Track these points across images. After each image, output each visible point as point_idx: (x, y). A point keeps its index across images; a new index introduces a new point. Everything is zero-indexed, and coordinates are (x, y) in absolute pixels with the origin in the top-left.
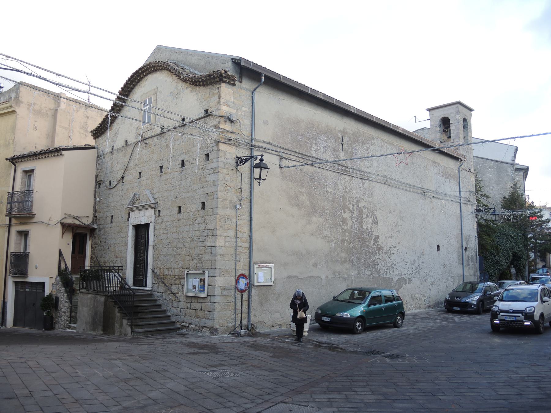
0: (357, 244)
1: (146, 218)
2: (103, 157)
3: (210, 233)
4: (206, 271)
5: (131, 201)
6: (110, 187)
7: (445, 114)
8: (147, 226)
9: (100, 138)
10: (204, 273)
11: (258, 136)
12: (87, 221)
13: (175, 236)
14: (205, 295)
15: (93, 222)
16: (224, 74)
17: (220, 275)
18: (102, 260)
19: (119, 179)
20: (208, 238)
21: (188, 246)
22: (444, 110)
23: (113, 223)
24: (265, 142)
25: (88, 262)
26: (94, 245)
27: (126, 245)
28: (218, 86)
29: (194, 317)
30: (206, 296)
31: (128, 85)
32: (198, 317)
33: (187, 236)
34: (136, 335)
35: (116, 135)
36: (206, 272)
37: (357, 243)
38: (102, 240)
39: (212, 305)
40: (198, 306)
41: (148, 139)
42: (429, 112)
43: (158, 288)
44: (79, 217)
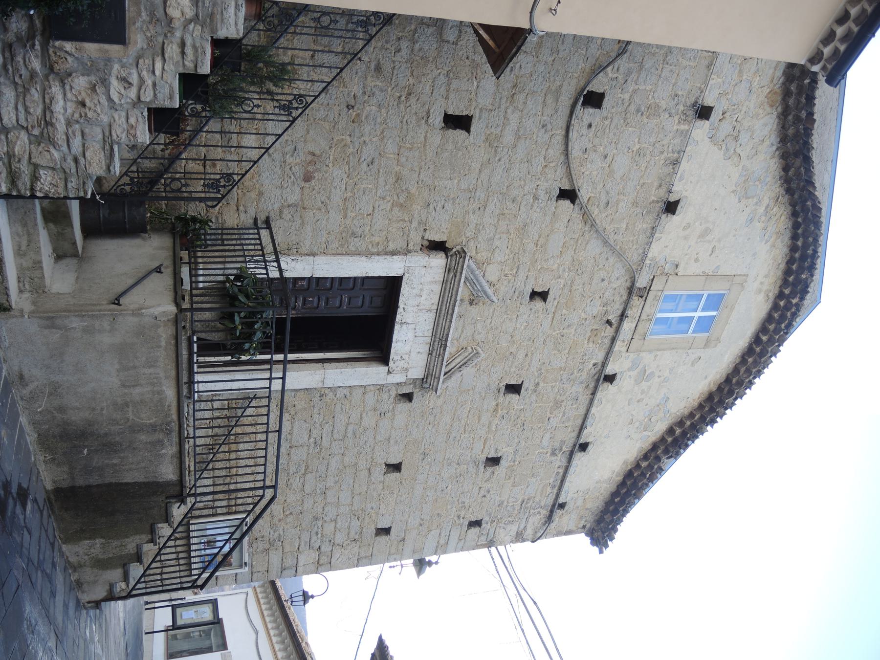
1: (407, 348)
21: (305, 508)
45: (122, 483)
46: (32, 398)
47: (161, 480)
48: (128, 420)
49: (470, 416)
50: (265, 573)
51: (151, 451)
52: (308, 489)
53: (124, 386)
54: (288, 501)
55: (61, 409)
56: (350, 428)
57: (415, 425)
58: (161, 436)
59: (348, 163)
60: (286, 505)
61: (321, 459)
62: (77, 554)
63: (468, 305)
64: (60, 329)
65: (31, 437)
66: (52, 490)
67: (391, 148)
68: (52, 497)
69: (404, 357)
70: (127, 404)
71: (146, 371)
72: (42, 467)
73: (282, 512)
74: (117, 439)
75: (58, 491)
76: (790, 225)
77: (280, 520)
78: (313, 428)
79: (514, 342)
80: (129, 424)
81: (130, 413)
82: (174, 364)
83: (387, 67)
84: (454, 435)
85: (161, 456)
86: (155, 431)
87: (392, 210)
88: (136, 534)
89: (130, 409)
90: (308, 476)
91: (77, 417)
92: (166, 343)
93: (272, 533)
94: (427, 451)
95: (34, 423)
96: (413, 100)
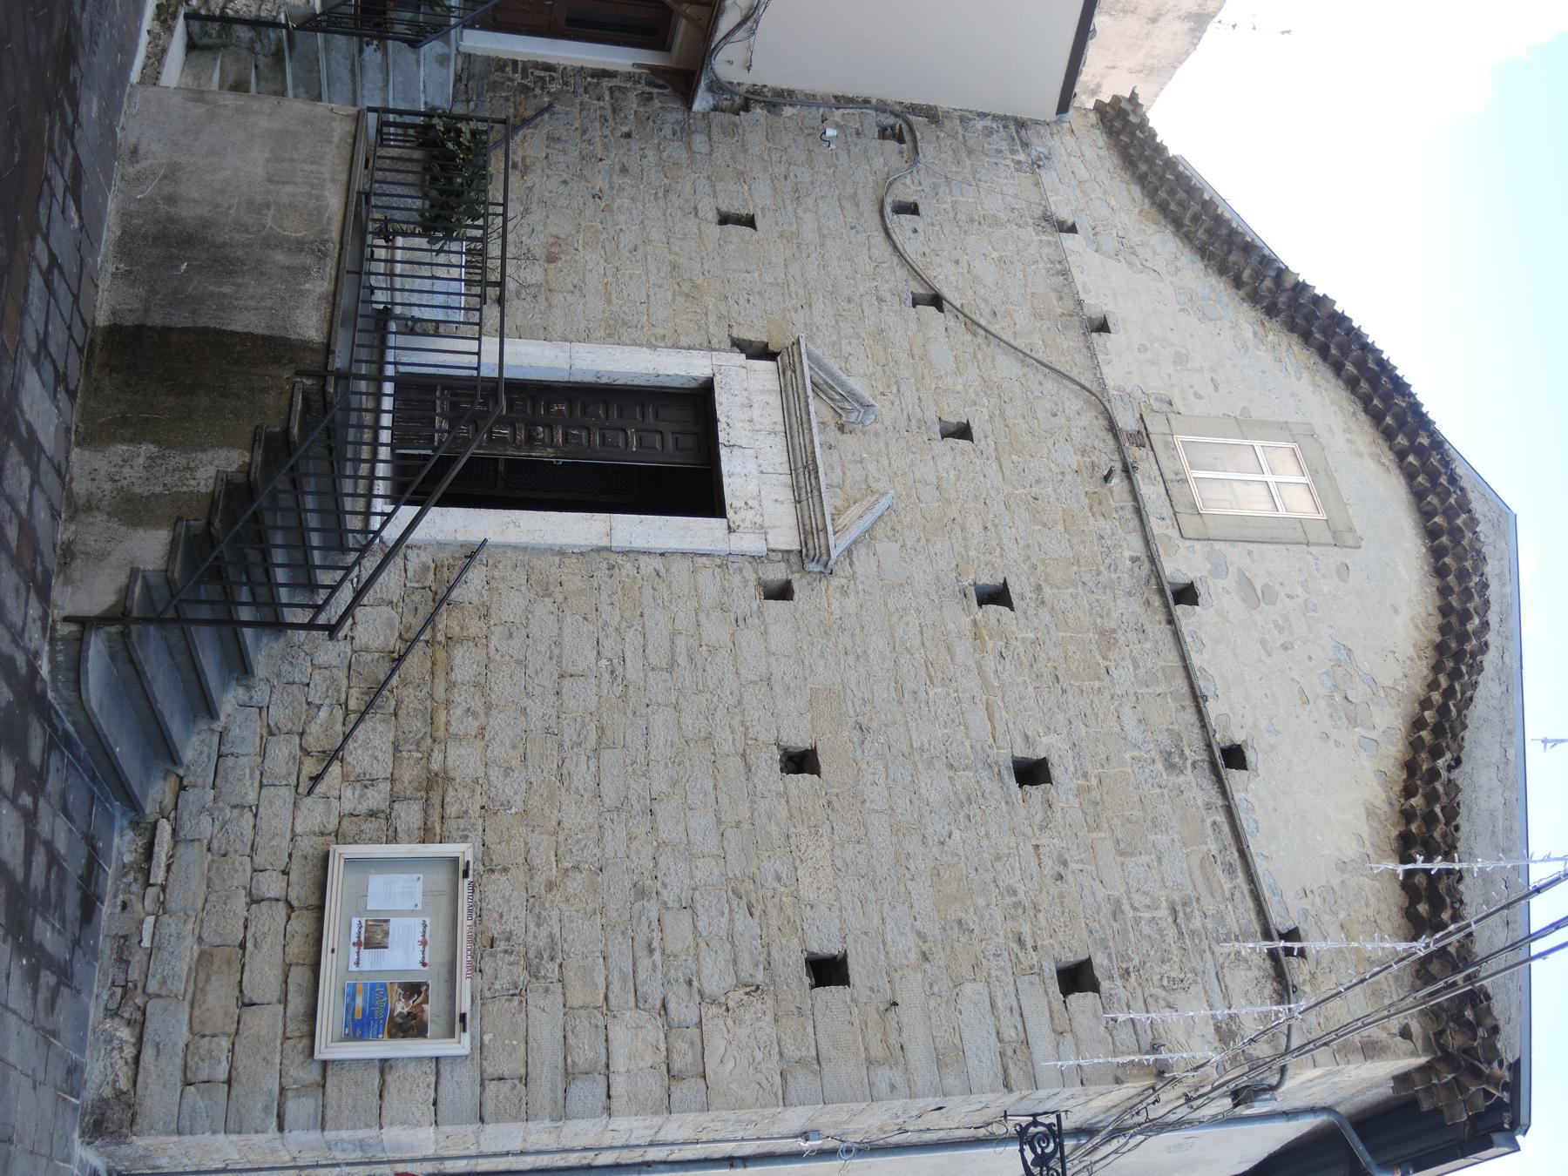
1: (752, 488)
2: (1022, 157)
4: (466, 1037)
5: (831, 375)
6: (888, 209)
9: (1101, 139)
10: (457, 1023)
12: (730, 62)
13: (661, 722)
14: (328, 1048)
15: (717, 87)
18: (529, 145)
19: (929, 274)
20: (653, 1032)
21: (610, 853)
23: (715, 231)
25: (527, 50)
26: (611, 90)
27: (614, 332)
29: (200, 939)
30: (328, 1048)
31: (1356, 352)
32: (202, 976)
33: (664, 836)
34: (60, 658)
35: (1125, 251)
36: (461, 1045)
38: (635, 145)
39: (266, 1109)
41: (1126, 482)
44: (752, 32)
45: (225, 331)
46: (139, 179)
47: (293, 337)
48: (264, 227)
49: (927, 643)
50: (520, 1086)
51: (288, 281)
52: (610, 795)
53: (270, 180)
54: (565, 824)
55: (171, 200)
56: (681, 642)
57: (816, 652)
58: (309, 260)
59: (604, 247)
60: (561, 838)
61: (630, 716)
62: (92, 475)
63: (838, 434)
64: (208, 104)
65: (110, 233)
66: (105, 327)
67: (656, 234)
68: (99, 340)
69: (751, 503)
70: (268, 206)
71: (305, 167)
72: (104, 283)
73: (553, 858)
74: (240, 253)
75: (114, 330)
76: (1315, 358)
77: (550, 886)
78: (602, 636)
79: (948, 501)
80: (263, 233)
81: (269, 219)
82: (347, 167)
83: (634, 168)
84: (909, 686)
85: (302, 293)
86: (301, 251)
87: (674, 300)
88: (220, 445)
89: (271, 212)
90: (607, 757)
91: (188, 213)
92: (341, 140)
93: (532, 927)
94: (864, 721)
95: (125, 215)
96: (672, 196)
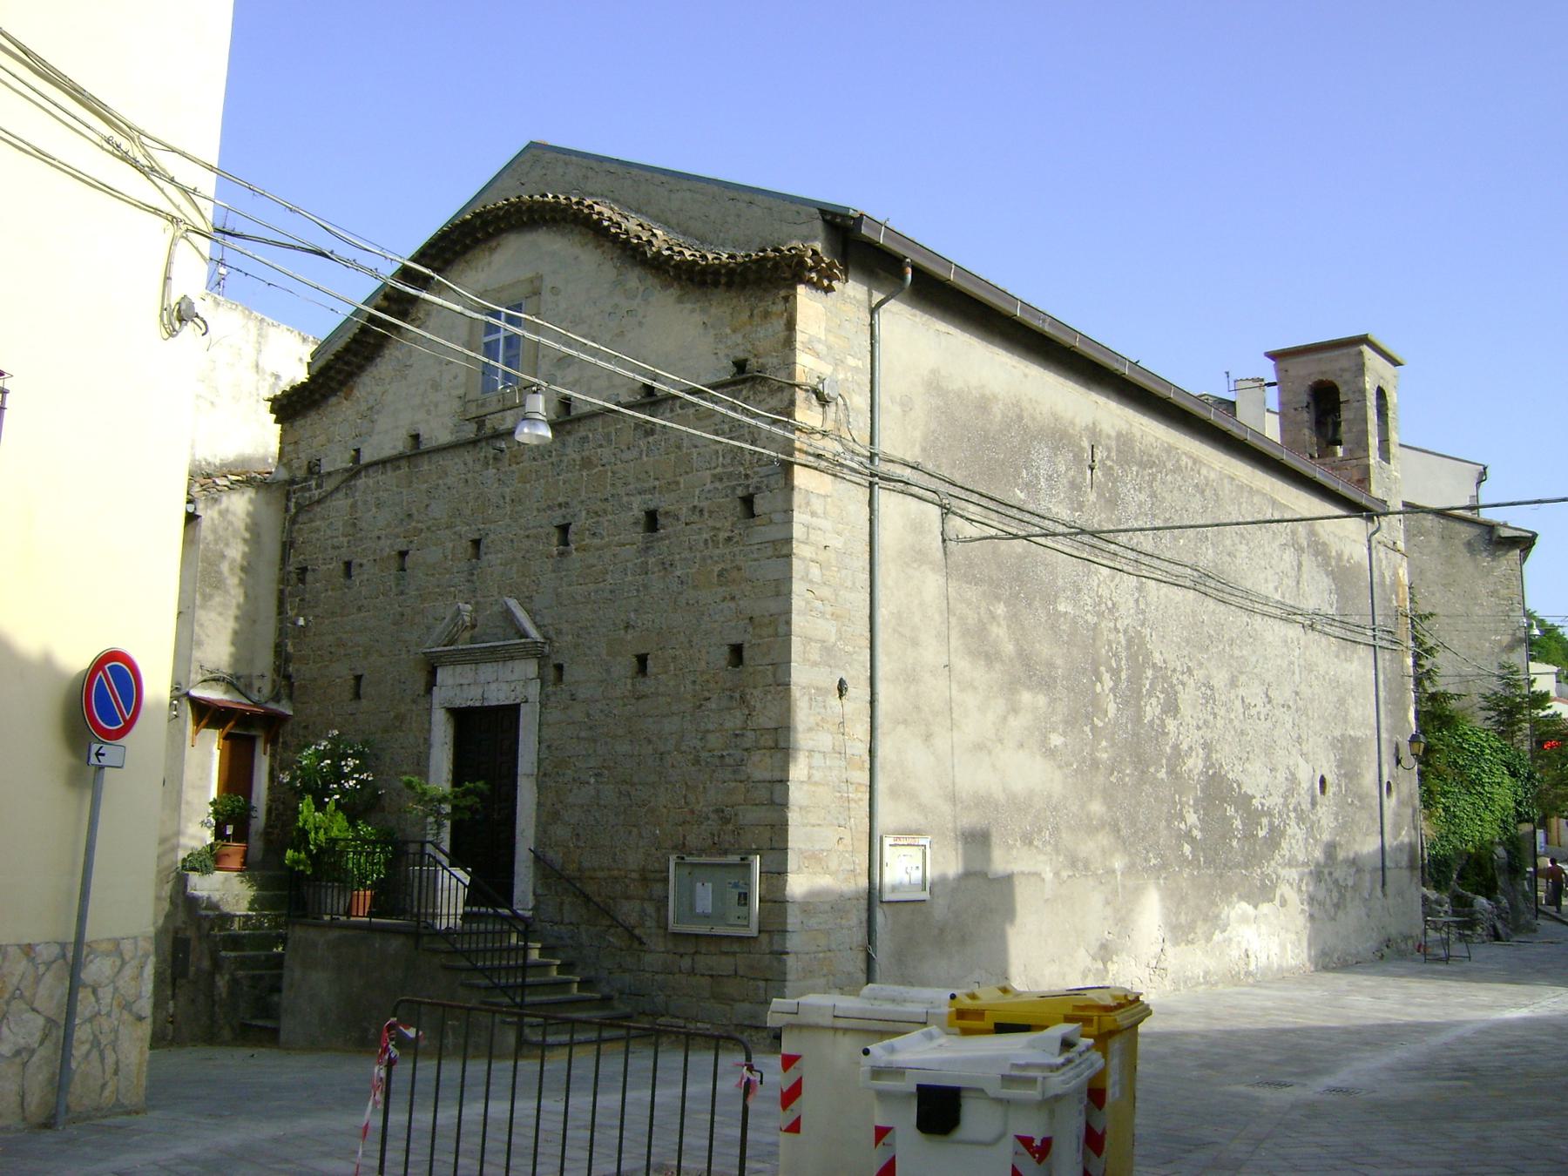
0: (1128, 775)
3: (767, 740)
7: (1323, 373)
8: (508, 715)
9: (299, 422)
11: (885, 445)
16: (810, 258)
17: (799, 867)
22: (1320, 360)
23: (364, 702)
24: (906, 465)
28: (783, 293)
30: (753, 931)
35: (370, 414)
37: (1128, 772)
40: (724, 964)
42: (1273, 363)
43: (561, 910)
